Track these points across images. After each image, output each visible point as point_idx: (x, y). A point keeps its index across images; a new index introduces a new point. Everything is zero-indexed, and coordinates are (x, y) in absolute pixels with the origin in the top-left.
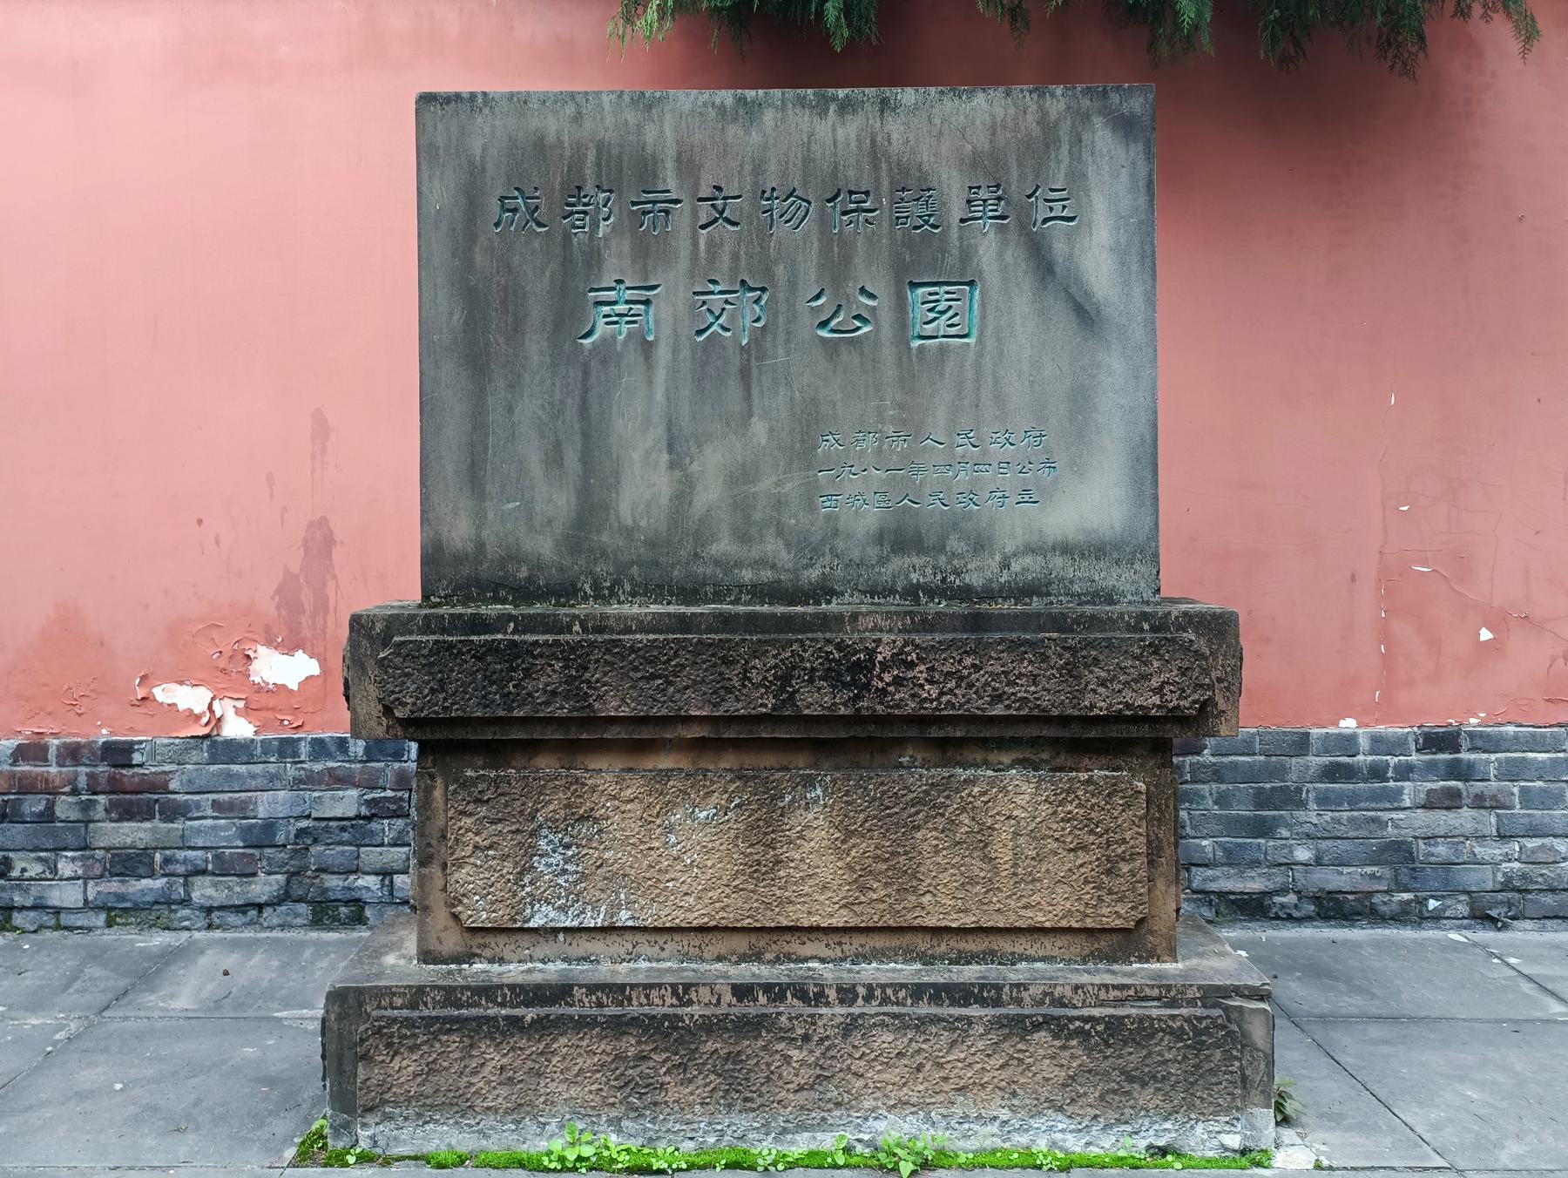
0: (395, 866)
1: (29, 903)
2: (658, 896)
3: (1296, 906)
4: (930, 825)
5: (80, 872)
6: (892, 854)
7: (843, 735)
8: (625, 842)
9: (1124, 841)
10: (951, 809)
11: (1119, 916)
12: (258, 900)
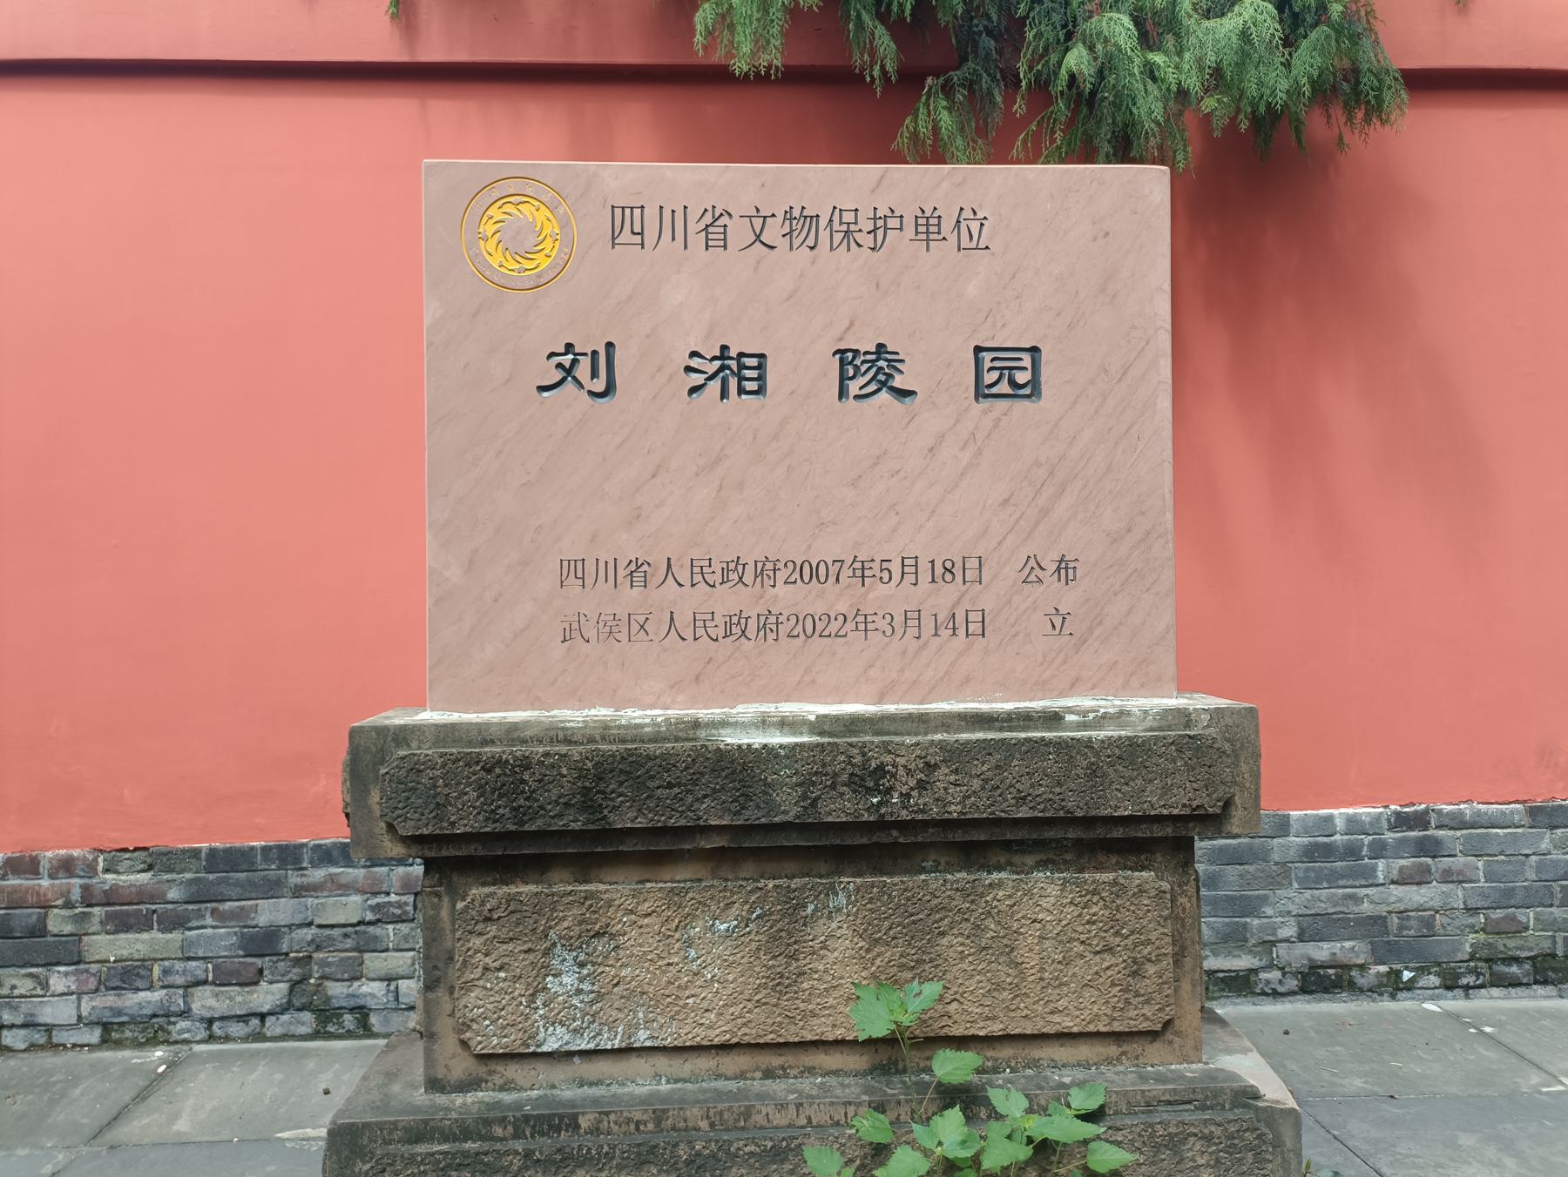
0: (401, 971)
1: (19, 1021)
2: (678, 1013)
3: (1280, 982)
4: (955, 931)
5: (73, 987)
6: (918, 962)
7: (864, 841)
8: (642, 958)
9: (1149, 942)
10: (976, 914)
11: (1147, 1019)
12: (260, 1010)
